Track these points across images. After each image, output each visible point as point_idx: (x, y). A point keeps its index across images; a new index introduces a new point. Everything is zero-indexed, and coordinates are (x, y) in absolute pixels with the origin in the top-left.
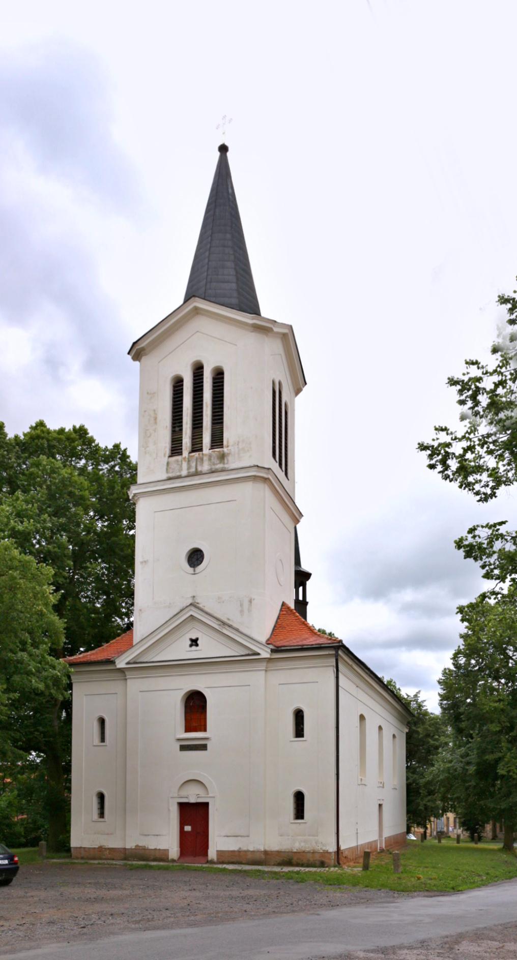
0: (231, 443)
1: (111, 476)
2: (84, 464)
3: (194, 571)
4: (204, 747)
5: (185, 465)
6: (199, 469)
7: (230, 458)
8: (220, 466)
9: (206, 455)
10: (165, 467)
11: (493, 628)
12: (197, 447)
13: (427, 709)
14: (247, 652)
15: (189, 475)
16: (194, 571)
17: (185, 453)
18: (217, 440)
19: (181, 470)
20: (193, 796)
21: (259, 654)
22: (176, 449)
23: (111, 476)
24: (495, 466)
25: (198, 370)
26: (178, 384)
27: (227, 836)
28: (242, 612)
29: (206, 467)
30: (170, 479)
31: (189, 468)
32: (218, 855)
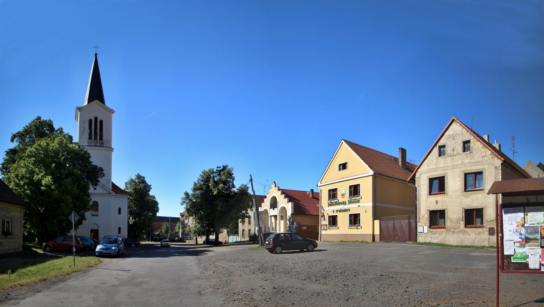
0: (105, 140)
1: (240, 197)
2: (51, 179)
4: (97, 215)
5: (93, 143)
6: (97, 145)
7: (104, 144)
8: (102, 145)
10: (87, 143)
11: (195, 208)
12: (96, 138)
13: (93, 164)
14: (108, 193)
15: (94, 146)
17: (98, 140)
18: (101, 138)
19: (92, 144)
20: (95, 228)
21: (112, 194)
22: (90, 138)
23: (240, 197)
24: (73, 141)
25: (96, 119)
26: (90, 121)
28: (107, 183)
29: (98, 145)
30: (88, 146)
31: (94, 144)
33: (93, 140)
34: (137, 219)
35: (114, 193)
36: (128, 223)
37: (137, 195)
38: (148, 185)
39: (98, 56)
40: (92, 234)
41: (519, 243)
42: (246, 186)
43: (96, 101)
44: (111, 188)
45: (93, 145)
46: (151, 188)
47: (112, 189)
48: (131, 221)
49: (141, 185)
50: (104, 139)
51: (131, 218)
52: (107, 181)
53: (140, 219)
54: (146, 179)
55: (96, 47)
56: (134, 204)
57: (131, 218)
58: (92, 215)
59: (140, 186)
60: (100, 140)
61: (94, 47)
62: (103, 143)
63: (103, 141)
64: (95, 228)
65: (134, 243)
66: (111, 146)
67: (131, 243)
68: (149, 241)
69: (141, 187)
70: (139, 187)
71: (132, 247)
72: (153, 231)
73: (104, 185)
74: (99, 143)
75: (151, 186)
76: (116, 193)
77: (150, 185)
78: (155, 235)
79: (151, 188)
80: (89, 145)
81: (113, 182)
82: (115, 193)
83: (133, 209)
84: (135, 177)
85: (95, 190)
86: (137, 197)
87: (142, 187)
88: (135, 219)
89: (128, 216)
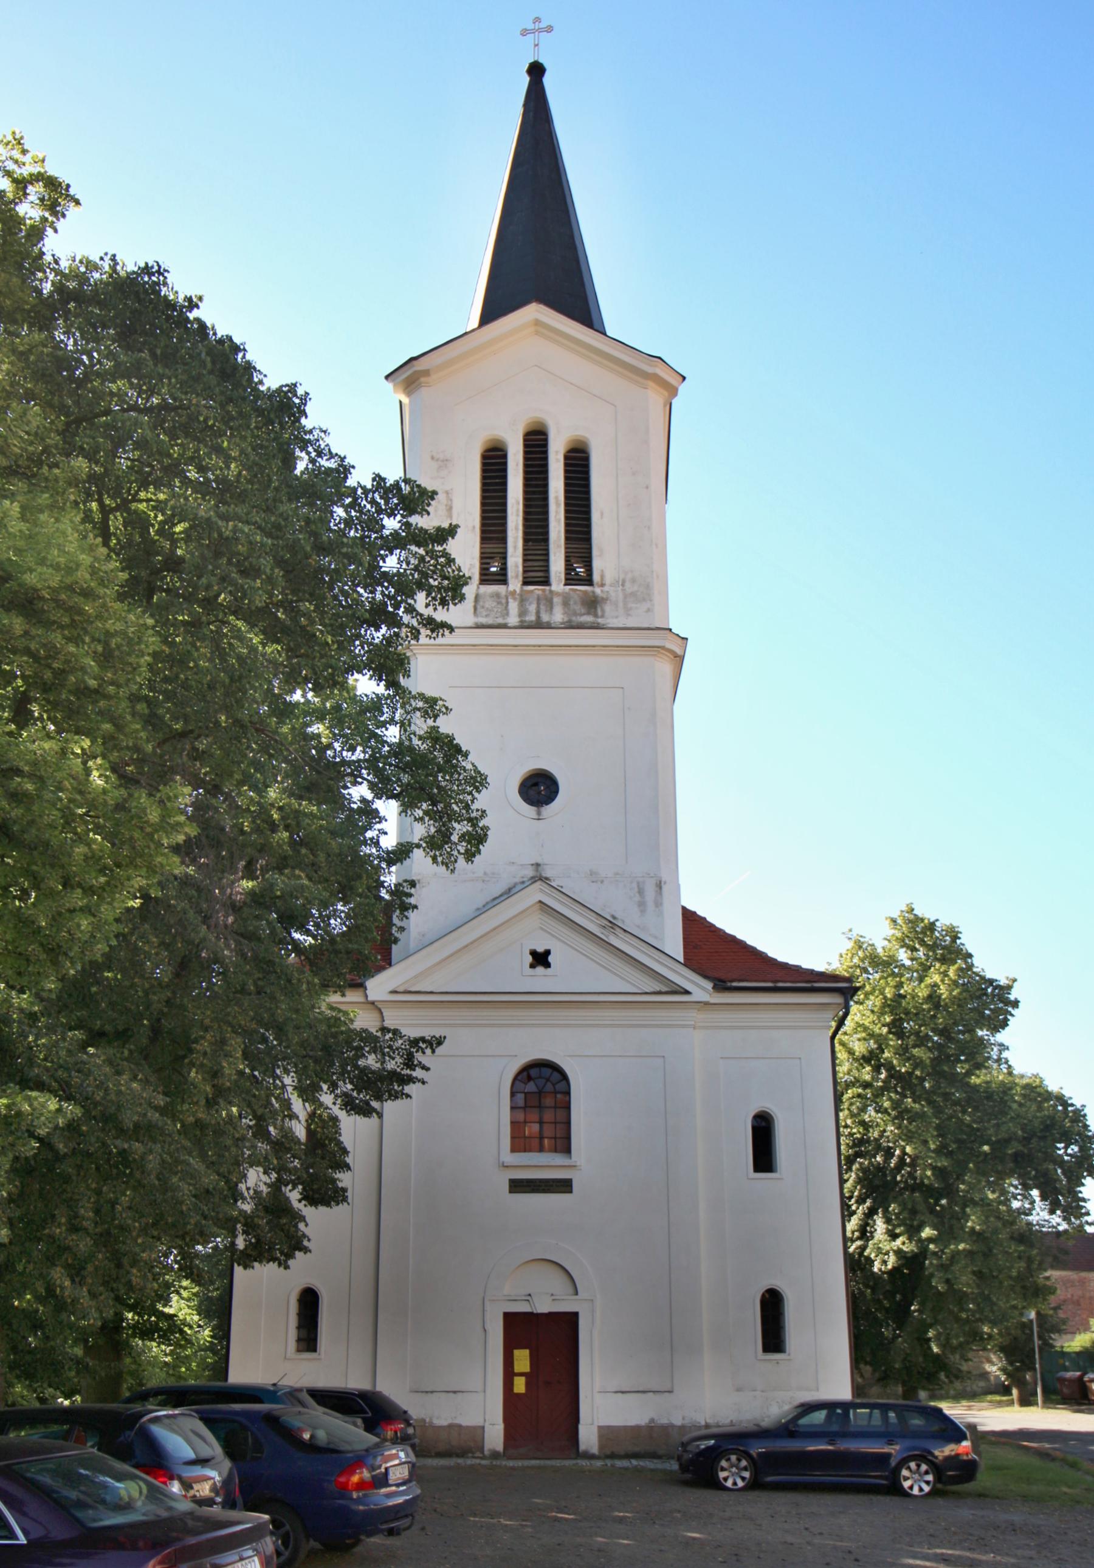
0: (608, 580)
3: (539, 813)
4: (564, 1186)
5: (514, 606)
6: (545, 618)
7: (608, 608)
8: (589, 619)
9: (558, 594)
16: (539, 813)
27: (623, 1392)
28: (642, 905)
30: (479, 626)
31: (522, 613)
32: (601, 1436)
33: (515, 583)
34: (927, 1232)
35: (700, 989)
36: (856, 1265)
37: (915, 1051)
38: (991, 982)
39: (547, 80)
40: (522, 1360)
41: (517, 1353)
42: (879, 1380)
43: (534, 312)
44: (675, 945)
45: (513, 619)
46: (1015, 1004)
47: (685, 959)
48: (879, 1251)
49: (937, 978)
50: (602, 577)
51: (880, 1226)
52: (641, 892)
53: (949, 1230)
54: (968, 941)
55: (539, 29)
56: (901, 1114)
57: (880, 1226)
58: (518, 1186)
59: (928, 981)
60: (571, 578)
61: (524, 33)
62: (592, 604)
63: (598, 590)
64: (543, 1307)
65: (924, 1457)
66: (667, 618)
67: (893, 1450)
68: (1027, 1401)
69: (935, 985)
70: (923, 992)
71: (905, 1494)
72: (1049, 1326)
73: (612, 924)
74: (566, 604)
75: (1009, 988)
76: (721, 985)
77: (1003, 982)
78: (1063, 1354)
79: (1015, 1004)
80: (483, 620)
81: (691, 907)
82: (709, 985)
83: (889, 1153)
84: (889, 931)
85: (540, 970)
86: (918, 1063)
87: (943, 991)
88: (913, 1232)
89: (842, 1182)
